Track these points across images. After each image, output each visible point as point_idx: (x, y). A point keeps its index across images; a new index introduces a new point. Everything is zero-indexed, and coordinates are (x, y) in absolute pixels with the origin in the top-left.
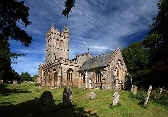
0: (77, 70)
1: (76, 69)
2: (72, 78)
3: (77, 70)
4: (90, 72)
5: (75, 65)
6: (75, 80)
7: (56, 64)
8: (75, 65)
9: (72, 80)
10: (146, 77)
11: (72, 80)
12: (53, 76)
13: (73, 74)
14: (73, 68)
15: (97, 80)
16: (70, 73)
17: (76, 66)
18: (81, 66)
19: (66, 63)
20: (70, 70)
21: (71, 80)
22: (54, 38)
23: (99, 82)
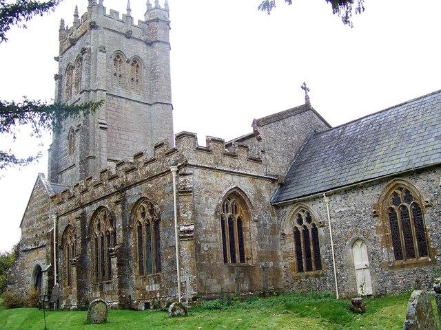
0: (267, 199)
1: (259, 192)
2: (241, 245)
3: (267, 199)
4: (371, 267)
5: (253, 170)
6: (261, 258)
7: (154, 168)
8: (253, 170)
9: (242, 259)
10: (364, 209)
11: (242, 259)
12: (132, 242)
13: (247, 224)
14: (246, 186)
15: (403, 244)
16: (230, 219)
17: (258, 177)
18: (284, 172)
19: (209, 161)
20: (236, 195)
21: (237, 256)
22: (103, 50)
23: (417, 253)
